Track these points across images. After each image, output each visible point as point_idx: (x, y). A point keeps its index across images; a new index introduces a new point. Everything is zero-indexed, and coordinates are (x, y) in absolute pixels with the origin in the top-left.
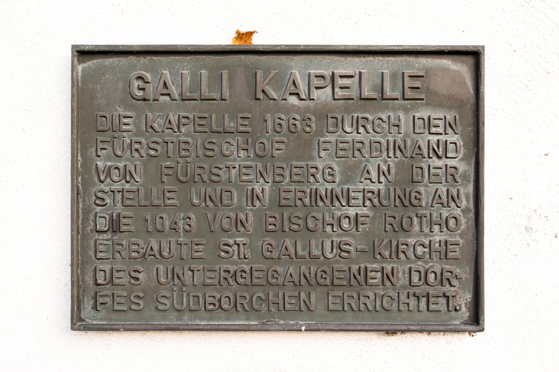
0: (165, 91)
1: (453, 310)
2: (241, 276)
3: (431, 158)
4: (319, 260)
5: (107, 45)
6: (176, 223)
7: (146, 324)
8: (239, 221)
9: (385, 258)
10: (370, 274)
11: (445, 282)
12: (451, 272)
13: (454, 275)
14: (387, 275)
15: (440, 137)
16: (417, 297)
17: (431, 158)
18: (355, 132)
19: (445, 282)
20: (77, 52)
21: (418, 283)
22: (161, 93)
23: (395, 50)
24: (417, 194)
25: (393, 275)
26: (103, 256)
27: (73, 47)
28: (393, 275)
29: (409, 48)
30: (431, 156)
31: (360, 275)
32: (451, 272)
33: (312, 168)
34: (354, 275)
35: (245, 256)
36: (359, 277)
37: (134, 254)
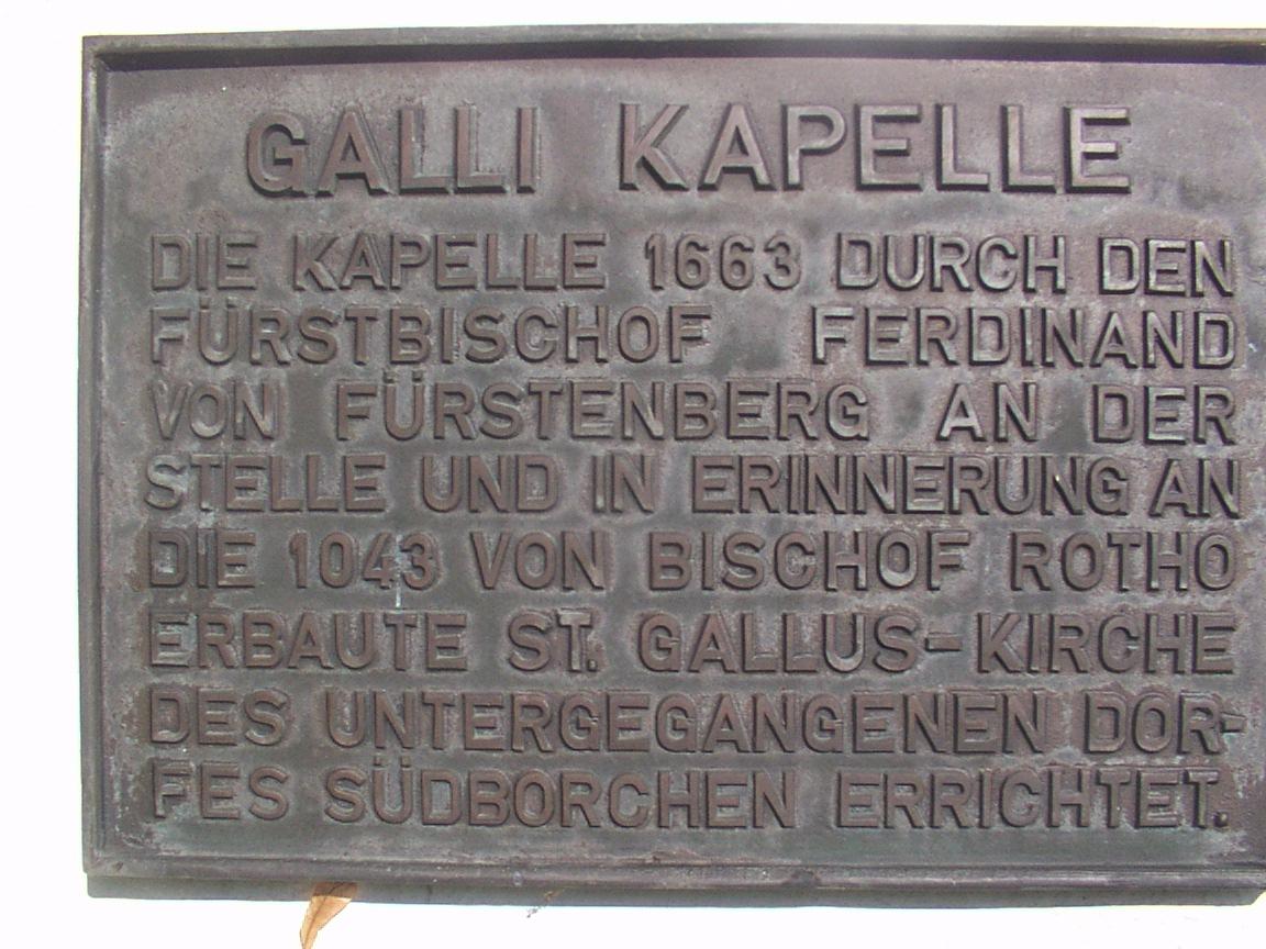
0: (352, 168)
1: (1211, 824)
2: (577, 722)
3: (925, 364)
4: (677, 674)
5: (1208, 30)
6: (380, 562)
7: (297, 860)
8: (569, 557)
9: (1011, 668)
10: (967, 720)
11: (1190, 742)
12: (1207, 711)
13: (1216, 719)
14: (1017, 719)
15: (1177, 303)
16: (1104, 785)
17: (925, 364)
18: (1018, 286)
19: (1190, 742)
20: (100, 55)
21: (1155, 744)
22: (339, 172)
23: (705, 37)
24: (1108, 477)
25: (1035, 722)
26: (174, 658)
27: (87, 40)
28: (1035, 722)
29: (572, 32)
30: (924, 357)
31: (936, 721)
32: (1207, 711)
33: (689, 394)
34: (919, 722)
35: (588, 663)
36: (934, 727)
37: (262, 656)
